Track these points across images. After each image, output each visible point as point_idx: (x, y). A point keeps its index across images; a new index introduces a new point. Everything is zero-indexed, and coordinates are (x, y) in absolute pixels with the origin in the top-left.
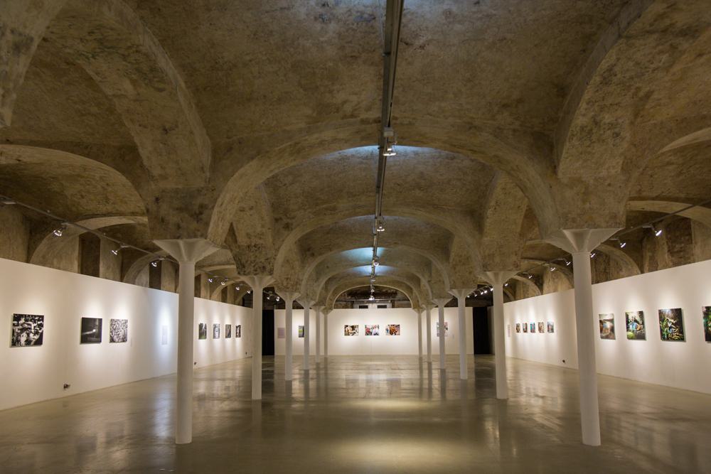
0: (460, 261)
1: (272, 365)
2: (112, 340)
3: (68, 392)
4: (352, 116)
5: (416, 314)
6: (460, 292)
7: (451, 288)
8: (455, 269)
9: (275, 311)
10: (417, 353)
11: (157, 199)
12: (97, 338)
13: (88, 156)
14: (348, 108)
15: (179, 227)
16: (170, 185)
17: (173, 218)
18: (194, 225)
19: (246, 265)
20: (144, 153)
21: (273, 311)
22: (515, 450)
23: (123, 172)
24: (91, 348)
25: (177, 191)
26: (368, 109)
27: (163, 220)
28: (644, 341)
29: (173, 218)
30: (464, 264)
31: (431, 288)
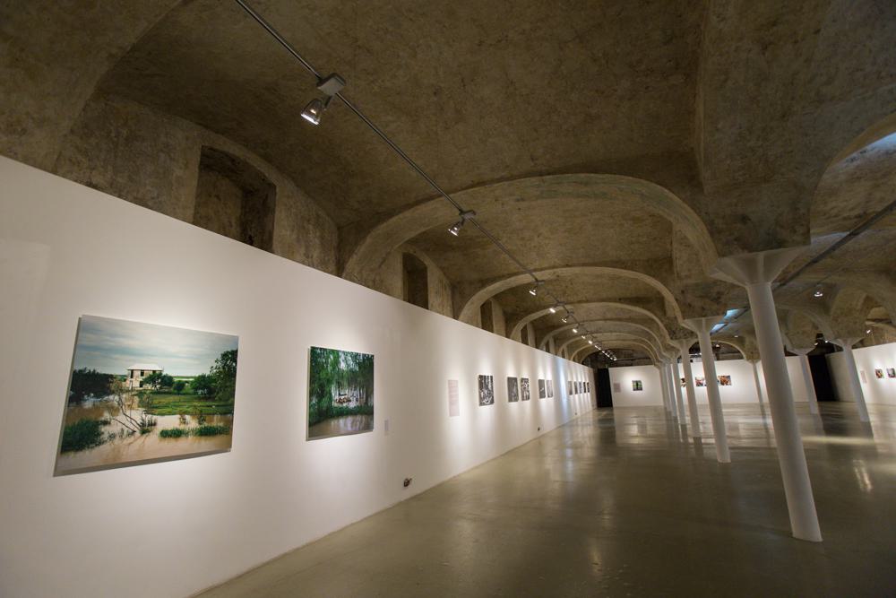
0: (842, 313)
1: (611, 420)
2: (523, 400)
3: (541, 433)
4: (836, 216)
5: (751, 365)
6: (845, 341)
7: (836, 338)
8: (837, 321)
9: (610, 369)
10: (757, 401)
11: (683, 292)
12: (544, 397)
13: (625, 268)
14: (834, 212)
15: (703, 309)
16: (691, 281)
17: (698, 304)
18: (715, 307)
19: (677, 332)
20: (678, 263)
21: (607, 370)
22: (596, 556)
23: (654, 276)
24: (513, 404)
25: (697, 285)
26: (852, 209)
27: (690, 305)
28: (52, 474)
29: (698, 304)
30: (846, 316)
31: (790, 340)
